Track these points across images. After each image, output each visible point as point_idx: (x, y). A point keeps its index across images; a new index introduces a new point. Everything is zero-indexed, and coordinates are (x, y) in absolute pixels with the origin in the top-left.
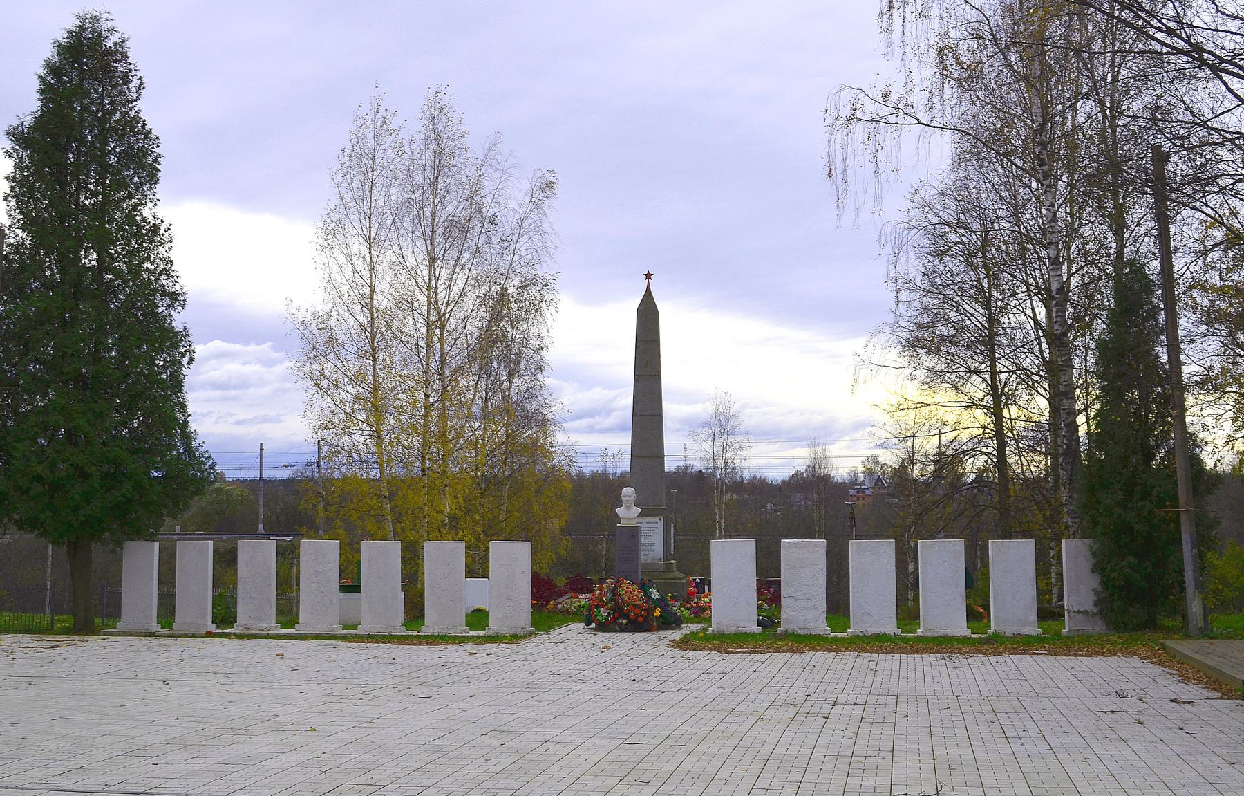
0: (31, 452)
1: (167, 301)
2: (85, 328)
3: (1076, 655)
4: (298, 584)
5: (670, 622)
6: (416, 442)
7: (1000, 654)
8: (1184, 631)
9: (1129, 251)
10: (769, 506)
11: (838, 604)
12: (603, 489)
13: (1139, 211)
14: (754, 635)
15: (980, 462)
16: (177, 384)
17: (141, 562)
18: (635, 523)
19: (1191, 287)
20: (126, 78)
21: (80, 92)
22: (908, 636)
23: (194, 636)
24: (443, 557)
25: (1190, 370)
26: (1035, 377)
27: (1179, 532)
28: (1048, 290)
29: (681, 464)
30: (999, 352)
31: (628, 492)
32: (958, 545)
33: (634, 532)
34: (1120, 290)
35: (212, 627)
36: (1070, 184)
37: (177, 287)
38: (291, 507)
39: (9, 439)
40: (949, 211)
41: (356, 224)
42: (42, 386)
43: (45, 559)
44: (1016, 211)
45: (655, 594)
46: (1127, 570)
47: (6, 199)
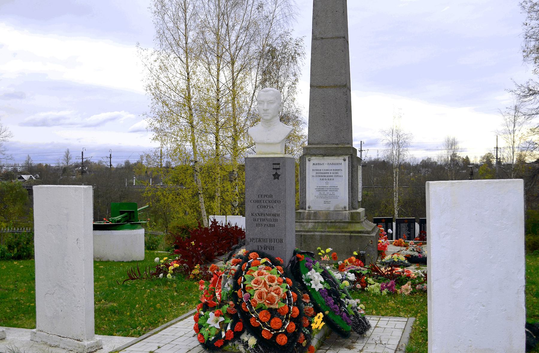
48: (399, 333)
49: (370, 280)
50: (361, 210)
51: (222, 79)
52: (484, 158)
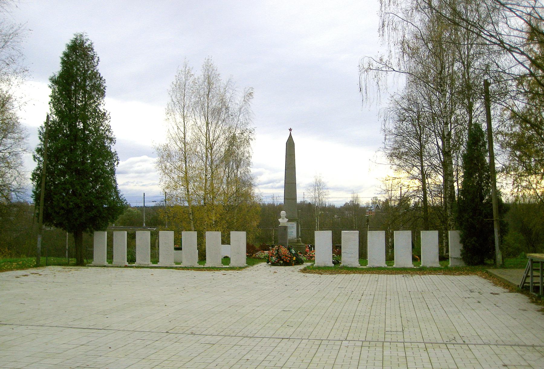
0: (60, 198)
1: (109, 141)
2: (79, 152)
3: (454, 275)
4: (158, 247)
5: (299, 262)
6: (202, 193)
7: (425, 274)
8: (494, 265)
9: (473, 121)
10: (336, 216)
11: (363, 255)
12: (272, 211)
13: (478, 105)
14: (331, 267)
15: (417, 200)
16: (113, 172)
17: (100, 239)
19: (497, 134)
20: (93, 58)
21: (76, 63)
22: (390, 268)
23: (120, 267)
24: (213, 238)
25: (498, 165)
26: (438, 168)
27: (493, 229)
28: (443, 134)
29: (302, 200)
30: (424, 158)
31: (283, 213)
32: (409, 233)
33: (285, 228)
34: (471, 135)
35: (127, 264)
36: (452, 94)
37: (113, 136)
38: (156, 218)
39: (52, 194)
40: (405, 105)
41: (179, 111)
42: (63, 173)
43: (66, 237)
44: (431, 104)
45: (293, 251)
46: (473, 242)
47: (49, 104)
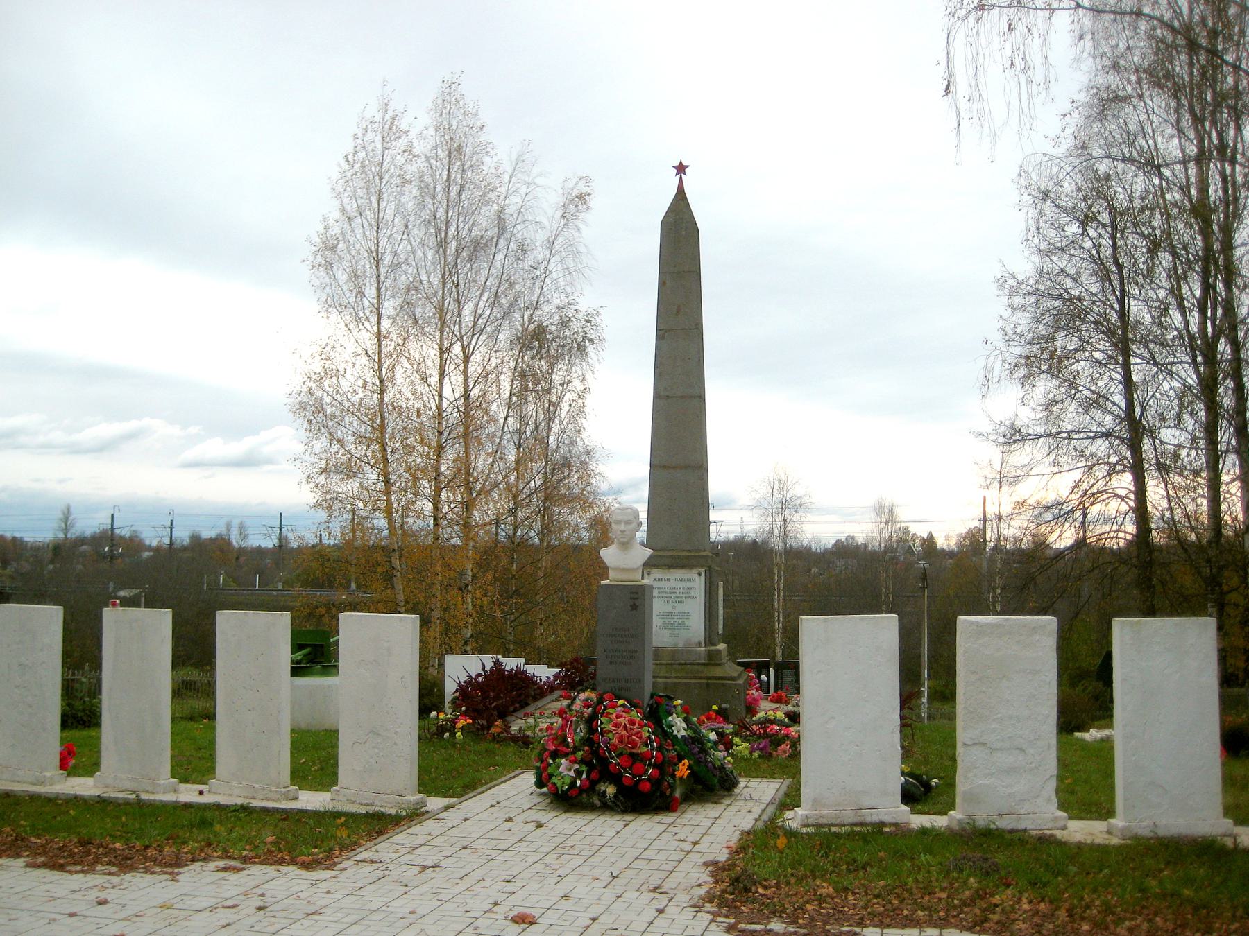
18: (636, 579)
48: (773, 792)
49: (737, 740)
50: (722, 646)
51: (447, 391)
52: (965, 538)
